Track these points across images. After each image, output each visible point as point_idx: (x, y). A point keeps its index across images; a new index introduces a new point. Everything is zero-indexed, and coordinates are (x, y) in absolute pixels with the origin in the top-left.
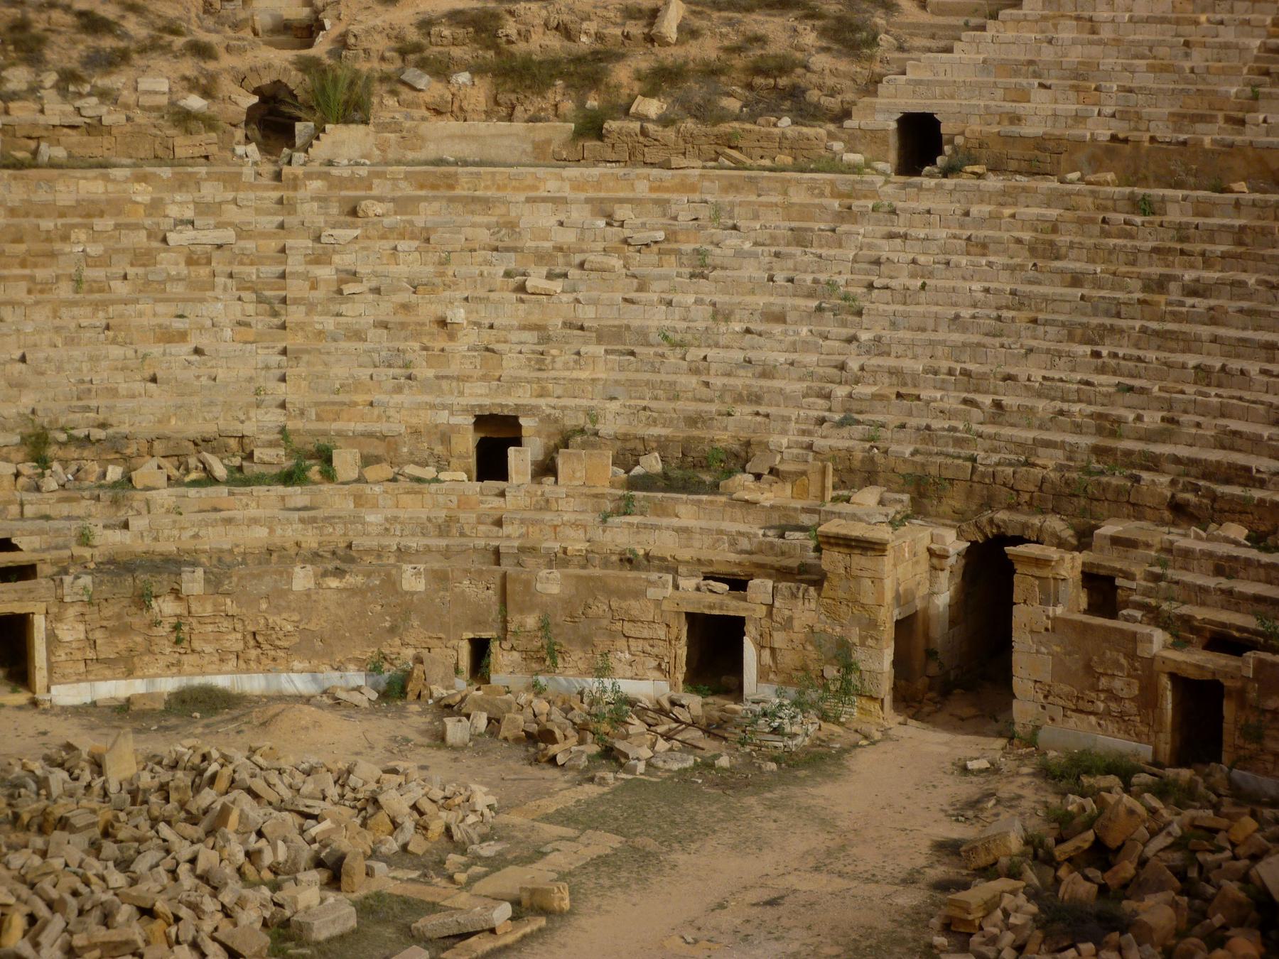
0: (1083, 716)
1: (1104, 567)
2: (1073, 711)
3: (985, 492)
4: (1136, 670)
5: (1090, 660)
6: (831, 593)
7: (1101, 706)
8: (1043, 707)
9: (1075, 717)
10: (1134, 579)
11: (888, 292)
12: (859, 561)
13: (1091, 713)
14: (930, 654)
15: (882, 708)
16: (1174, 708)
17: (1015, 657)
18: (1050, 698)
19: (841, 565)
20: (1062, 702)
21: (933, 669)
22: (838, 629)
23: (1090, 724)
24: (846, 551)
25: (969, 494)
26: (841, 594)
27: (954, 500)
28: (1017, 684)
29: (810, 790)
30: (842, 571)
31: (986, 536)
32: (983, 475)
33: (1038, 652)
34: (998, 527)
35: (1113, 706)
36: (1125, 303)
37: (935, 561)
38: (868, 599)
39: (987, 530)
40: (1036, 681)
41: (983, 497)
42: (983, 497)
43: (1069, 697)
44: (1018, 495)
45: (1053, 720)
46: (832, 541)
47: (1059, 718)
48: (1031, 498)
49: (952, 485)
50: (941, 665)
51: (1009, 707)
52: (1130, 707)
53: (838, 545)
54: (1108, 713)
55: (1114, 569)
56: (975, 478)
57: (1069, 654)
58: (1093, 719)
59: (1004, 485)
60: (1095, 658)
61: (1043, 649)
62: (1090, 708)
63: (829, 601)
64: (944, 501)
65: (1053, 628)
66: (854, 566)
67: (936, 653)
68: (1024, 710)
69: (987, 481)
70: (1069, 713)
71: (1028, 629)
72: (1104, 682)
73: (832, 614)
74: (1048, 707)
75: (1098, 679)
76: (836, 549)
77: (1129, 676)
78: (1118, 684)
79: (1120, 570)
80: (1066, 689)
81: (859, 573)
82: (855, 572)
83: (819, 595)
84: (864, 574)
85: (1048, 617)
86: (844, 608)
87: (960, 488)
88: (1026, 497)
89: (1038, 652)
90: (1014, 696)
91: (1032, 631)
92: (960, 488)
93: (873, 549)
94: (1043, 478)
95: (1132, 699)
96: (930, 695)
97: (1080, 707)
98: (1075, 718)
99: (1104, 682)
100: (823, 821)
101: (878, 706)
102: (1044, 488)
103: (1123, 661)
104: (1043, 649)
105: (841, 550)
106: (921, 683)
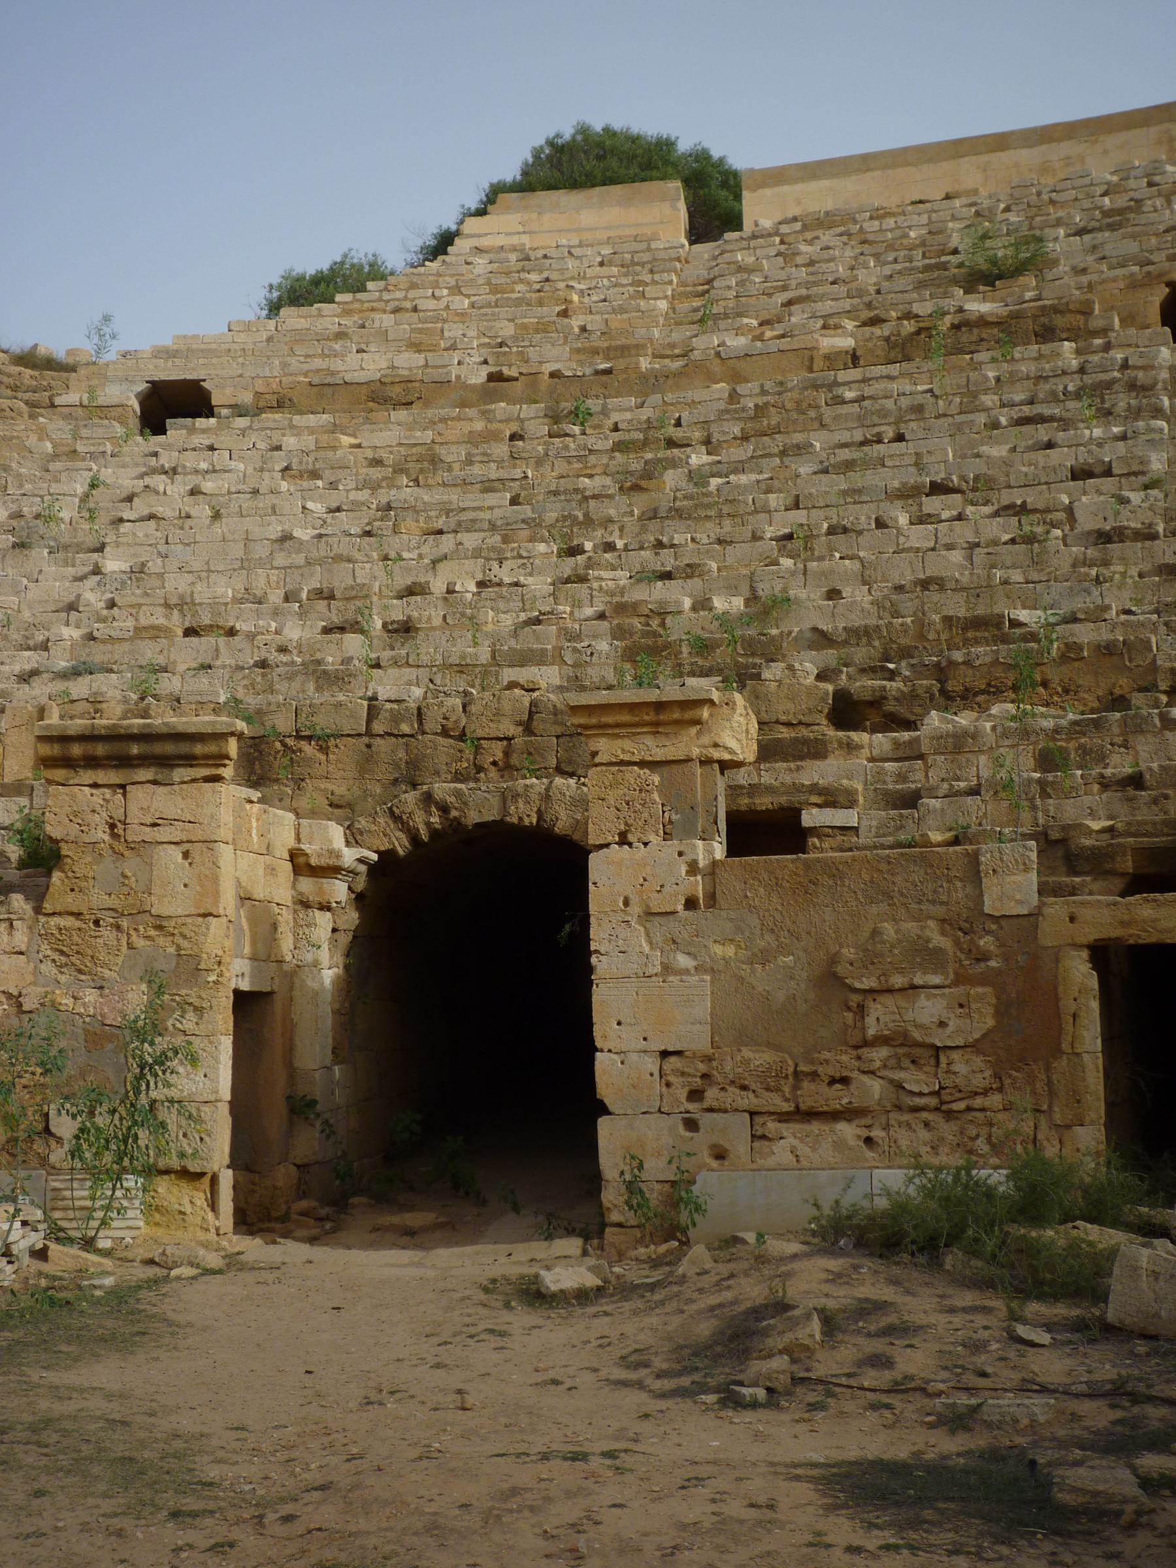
0: (816, 1127)
1: (770, 789)
2: (783, 1117)
3: (401, 754)
4: (983, 957)
5: (834, 960)
6: (71, 901)
7: (875, 1088)
8: (691, 1124)
9: (791, 1137)
10: (851, 804)
11: (152, 523)
12: (149, 800)
13: (834, 1116)
14: (300, 1108)
15: (213, 1206)
16: (1108, 1038)
17: (599, 995)
18: (712, 1095)
19: (100, 820)
20: (748, 1100)
21: (308, 1143)
22: (90, 996)
23: (839, 1145)
24: (113, 776)
25: (366, 763)
26: (98, 898)
27: (336, 774)
28: (608, 1072)
29: (35, 1375)
30: (102, 835)
31: (415, 839)
32: (396, 718)
33: (667, 969)
34: (444, 809)
35: (916, 1080)
36: (594, 497)
37: (307, 885)
38: (172, 903)
39: (419, 821)
40: (665, 1054)
41: (396, 765)
42: (396, 765)
43: (771, 1080)
44: (478, 749)
45: (720, 1155)
46: (76, 750)
47: (740, 1145)
48: (507, 754)
49: (324, 750)
50: (329, 1130)
51: (587, 1146)
52: (968, 1070)
53: (92, 762)
54: (901, 1102)
55: (798, 788)
56: (378, 727)
57: (764, 957)
58: (847, 1130)
59: (445, 732)
60: (848, 953)
61: (683, 961)
62: (840, 1098)
63: (69, 922)
64: (309, 784)
65: (712, 899)
66: (135, 816)
67: (313, 1103)
68: (632, 1137)
69: (405, 728)
70: (772, 1126)
71: (636, 909)
72: (879, 1017)
73: (72, 957)
74: (705, 1120)
75: (861, 1010)
76: (88, 776)
77: (960, 979)
78: (927, 1010)
79: (814, 789)
80: (761, 1058)
81: (149, 834)
82: (136, 833)
83: (38, 910)
84: (163, 834)
85: (693, 869)
86: (108, 934)
87: (345, 752)
88: (497, 751)
89: (667, 969)
90: (604, 1110)
91: (649, 914)
92: (345, 752)
93: (190, 760)
94: (533, 704)
95: (973, 1047)
96: (304, 1204)
97: (806, 1104)
98: (790, 1141)
99: (879, 1017)
100: (129, 1470)
101: (200, 1199)
102: (537, 725)
103: (939, 940)
104: (683, 961)
105: (101, 776)
106: (283, 1176)
